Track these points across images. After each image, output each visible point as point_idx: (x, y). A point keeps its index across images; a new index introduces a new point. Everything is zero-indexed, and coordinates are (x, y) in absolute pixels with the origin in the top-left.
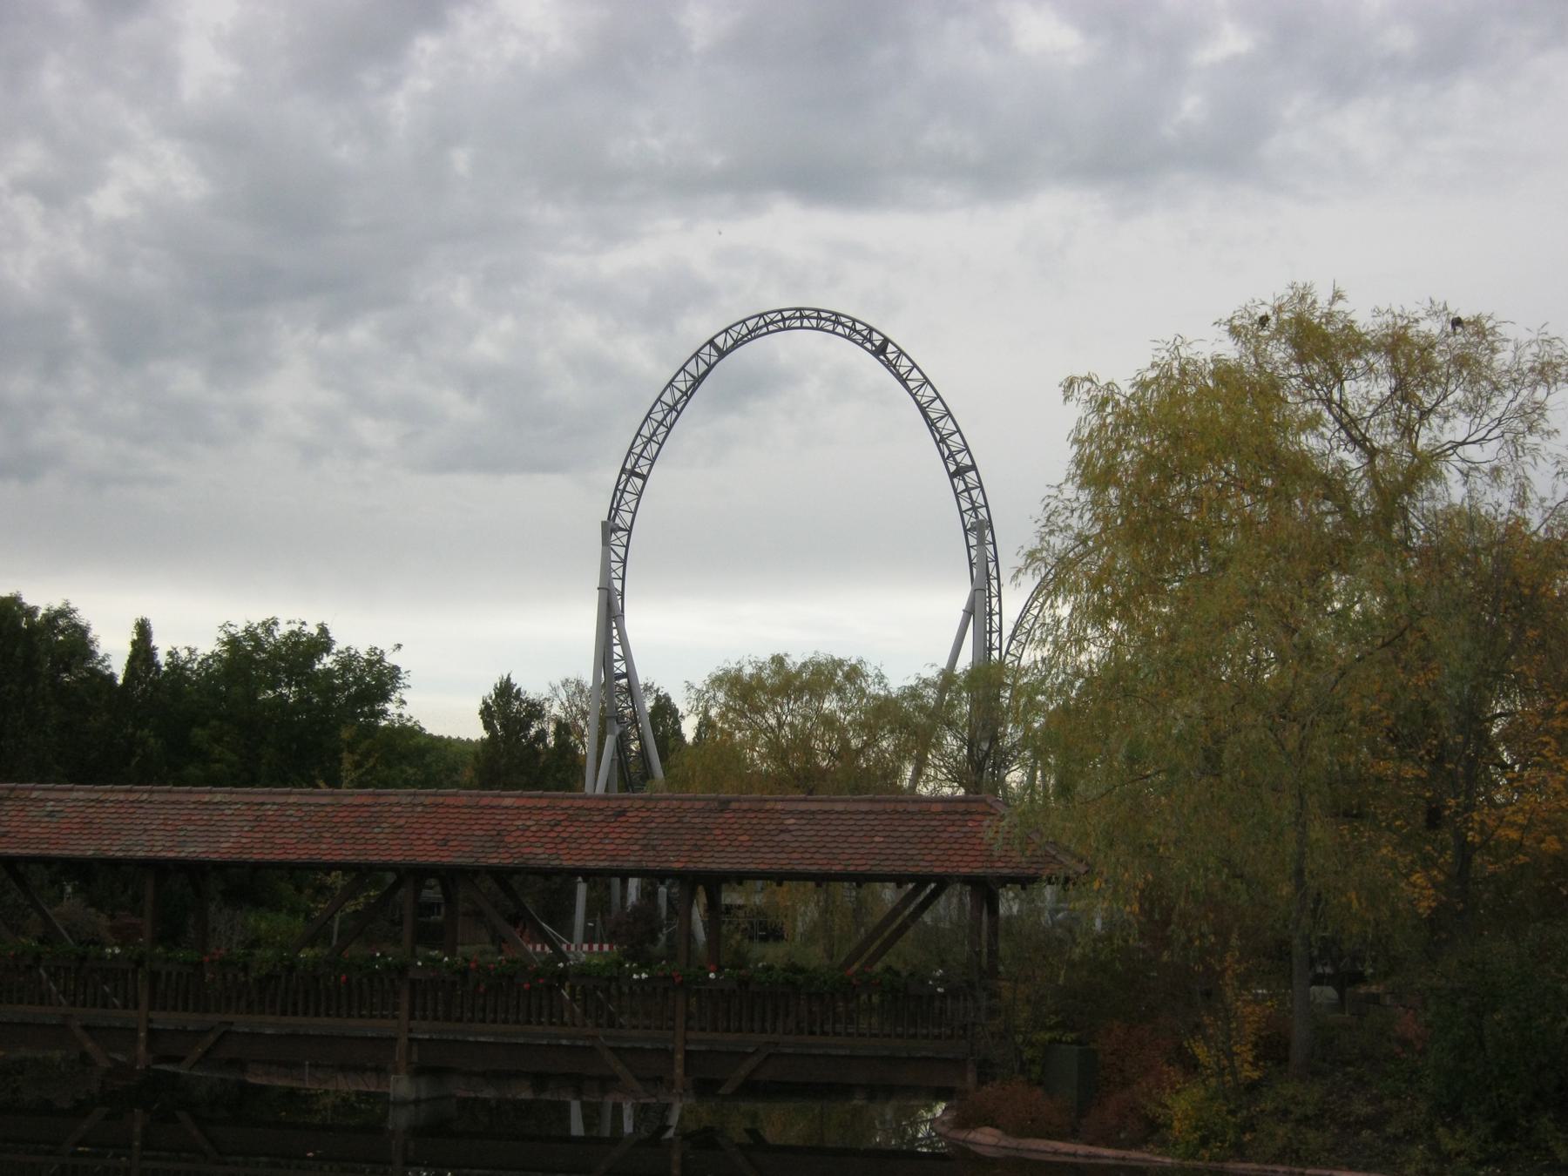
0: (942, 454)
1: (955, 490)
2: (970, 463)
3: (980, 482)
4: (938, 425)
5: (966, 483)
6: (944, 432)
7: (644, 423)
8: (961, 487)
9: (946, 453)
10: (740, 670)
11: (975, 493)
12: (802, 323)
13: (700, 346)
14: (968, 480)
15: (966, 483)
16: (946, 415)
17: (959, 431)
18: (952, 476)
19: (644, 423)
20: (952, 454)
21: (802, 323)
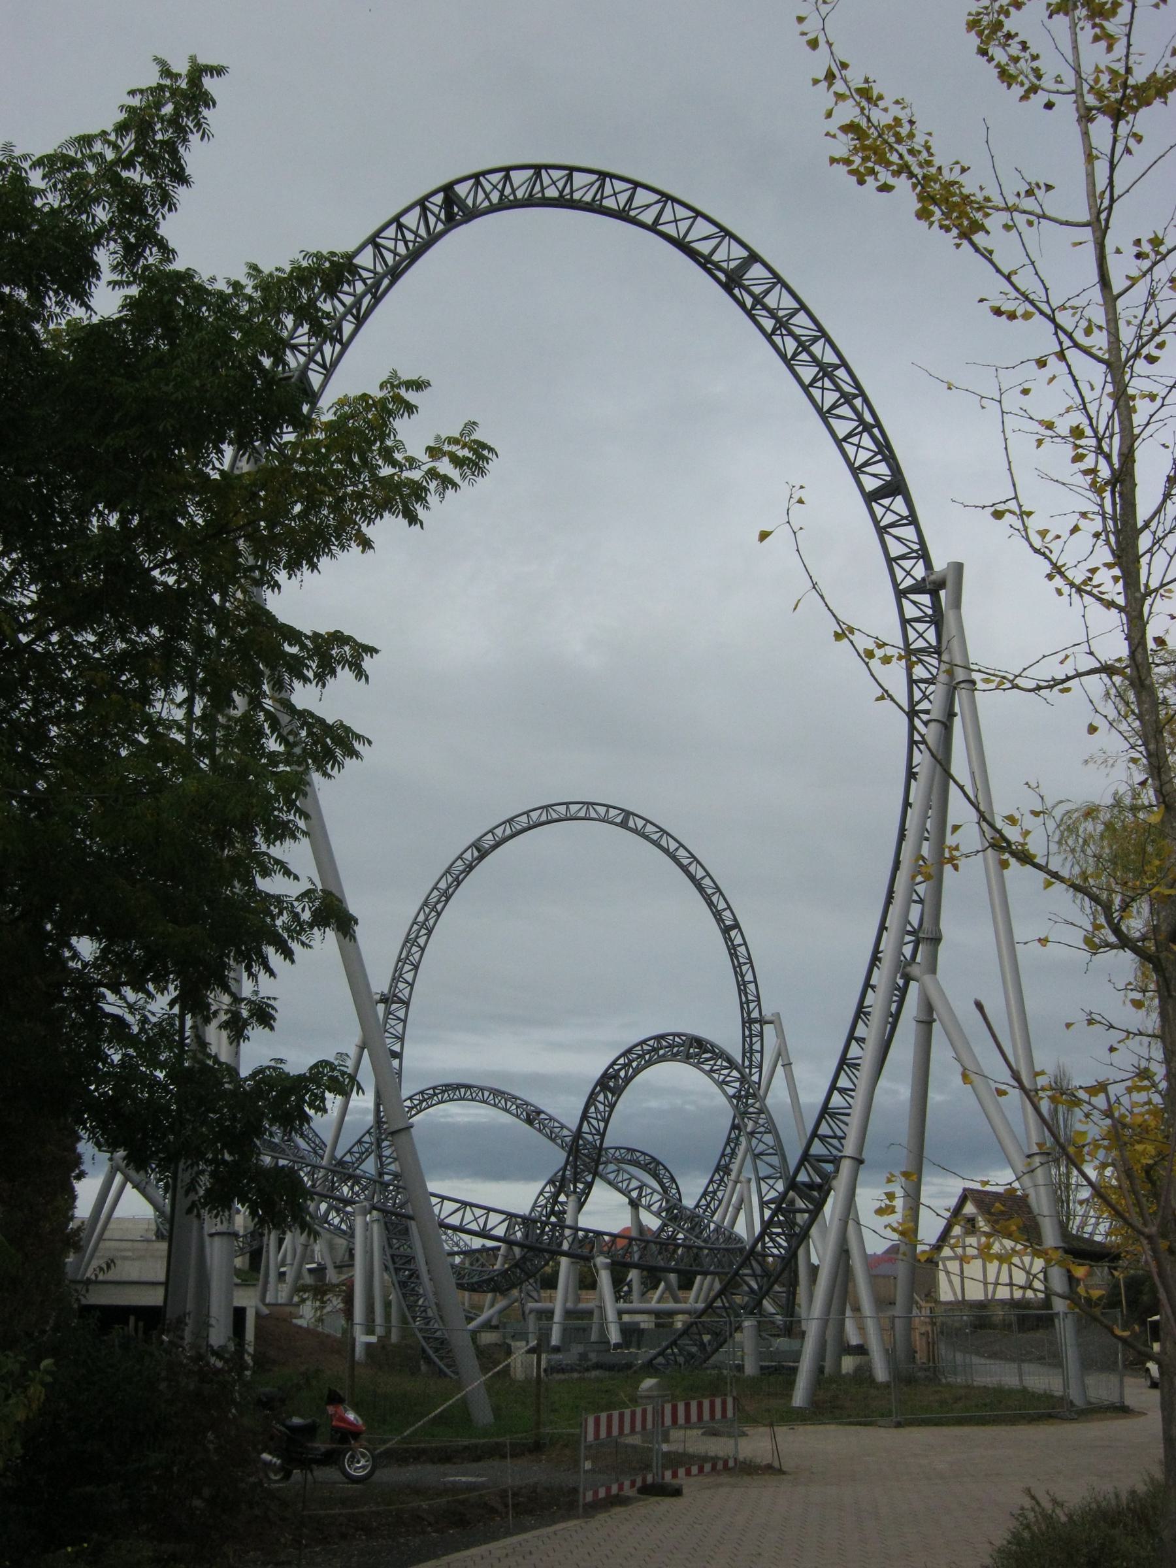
0: (742, 305)
1: (783, 356)
2: (745, 254)
3: (820, 328)
4: (715, 258)
5: (796, 338)
6: (781, 313)
7: (441, 878)
8: (791, 345)
9: (749, 301)
10: (1152, 1479)
11: (817, 349)
12: (724, 910)
13: (407, 930)
14: (798, 331)
15: (796, 338)
16: (775, 284)
17: (803, 307)
18: (728, 288)
19: (441, 878)
20: (758, 300)
21: (724, 910)
